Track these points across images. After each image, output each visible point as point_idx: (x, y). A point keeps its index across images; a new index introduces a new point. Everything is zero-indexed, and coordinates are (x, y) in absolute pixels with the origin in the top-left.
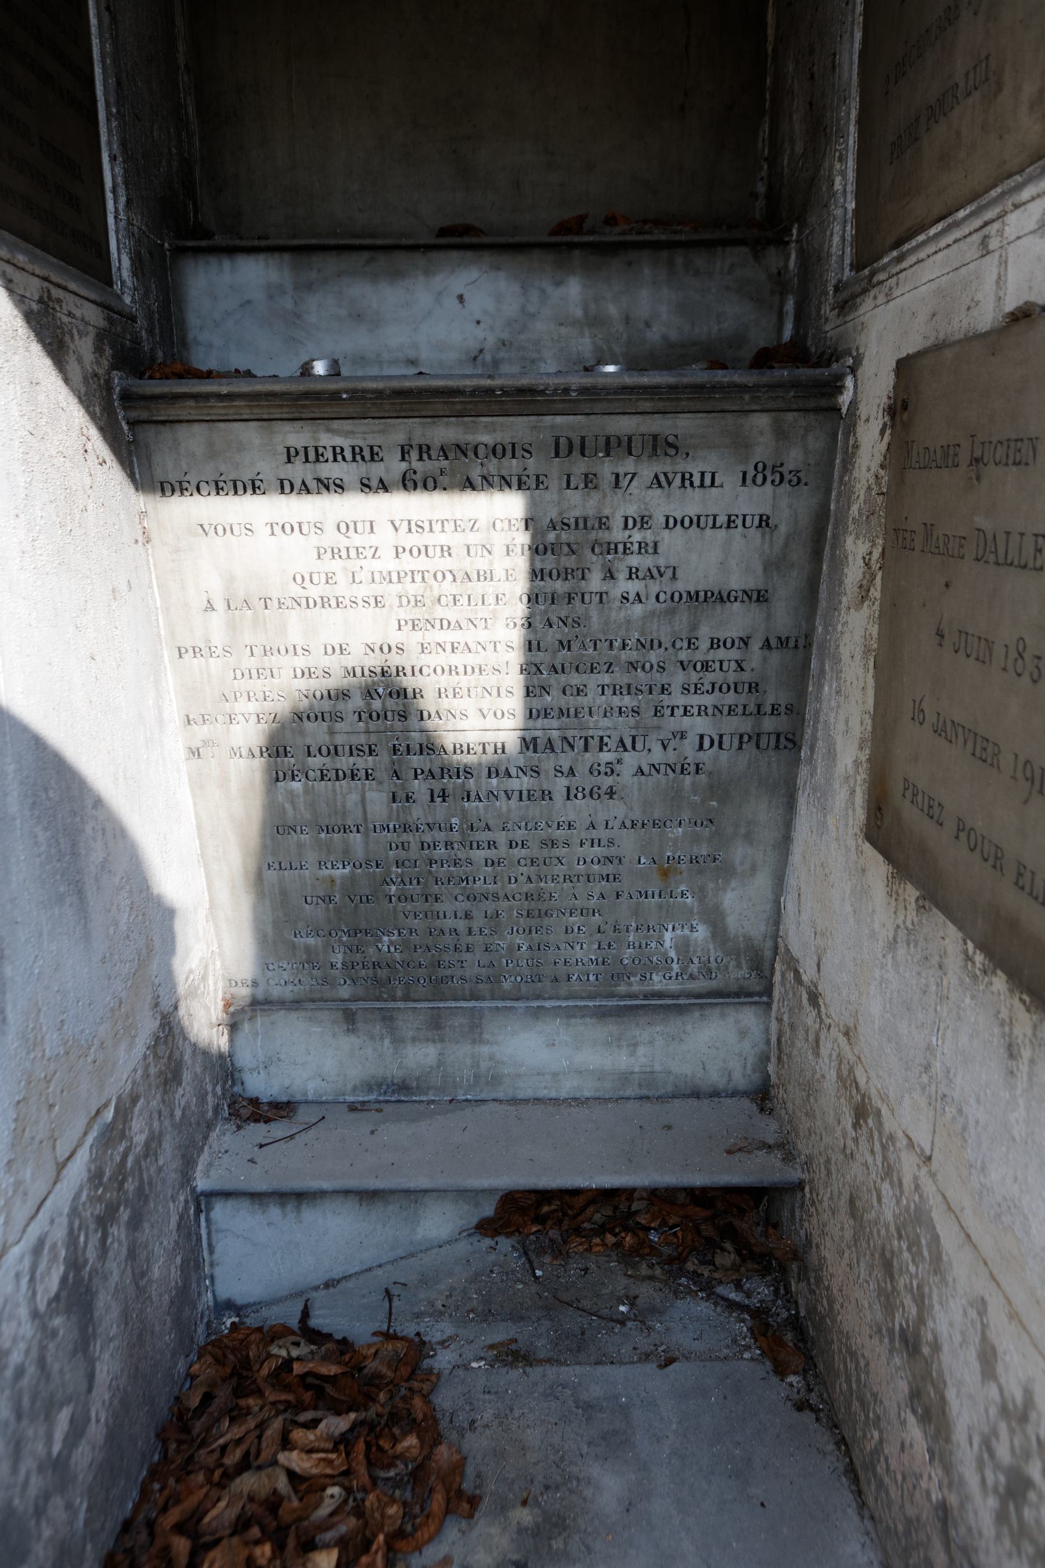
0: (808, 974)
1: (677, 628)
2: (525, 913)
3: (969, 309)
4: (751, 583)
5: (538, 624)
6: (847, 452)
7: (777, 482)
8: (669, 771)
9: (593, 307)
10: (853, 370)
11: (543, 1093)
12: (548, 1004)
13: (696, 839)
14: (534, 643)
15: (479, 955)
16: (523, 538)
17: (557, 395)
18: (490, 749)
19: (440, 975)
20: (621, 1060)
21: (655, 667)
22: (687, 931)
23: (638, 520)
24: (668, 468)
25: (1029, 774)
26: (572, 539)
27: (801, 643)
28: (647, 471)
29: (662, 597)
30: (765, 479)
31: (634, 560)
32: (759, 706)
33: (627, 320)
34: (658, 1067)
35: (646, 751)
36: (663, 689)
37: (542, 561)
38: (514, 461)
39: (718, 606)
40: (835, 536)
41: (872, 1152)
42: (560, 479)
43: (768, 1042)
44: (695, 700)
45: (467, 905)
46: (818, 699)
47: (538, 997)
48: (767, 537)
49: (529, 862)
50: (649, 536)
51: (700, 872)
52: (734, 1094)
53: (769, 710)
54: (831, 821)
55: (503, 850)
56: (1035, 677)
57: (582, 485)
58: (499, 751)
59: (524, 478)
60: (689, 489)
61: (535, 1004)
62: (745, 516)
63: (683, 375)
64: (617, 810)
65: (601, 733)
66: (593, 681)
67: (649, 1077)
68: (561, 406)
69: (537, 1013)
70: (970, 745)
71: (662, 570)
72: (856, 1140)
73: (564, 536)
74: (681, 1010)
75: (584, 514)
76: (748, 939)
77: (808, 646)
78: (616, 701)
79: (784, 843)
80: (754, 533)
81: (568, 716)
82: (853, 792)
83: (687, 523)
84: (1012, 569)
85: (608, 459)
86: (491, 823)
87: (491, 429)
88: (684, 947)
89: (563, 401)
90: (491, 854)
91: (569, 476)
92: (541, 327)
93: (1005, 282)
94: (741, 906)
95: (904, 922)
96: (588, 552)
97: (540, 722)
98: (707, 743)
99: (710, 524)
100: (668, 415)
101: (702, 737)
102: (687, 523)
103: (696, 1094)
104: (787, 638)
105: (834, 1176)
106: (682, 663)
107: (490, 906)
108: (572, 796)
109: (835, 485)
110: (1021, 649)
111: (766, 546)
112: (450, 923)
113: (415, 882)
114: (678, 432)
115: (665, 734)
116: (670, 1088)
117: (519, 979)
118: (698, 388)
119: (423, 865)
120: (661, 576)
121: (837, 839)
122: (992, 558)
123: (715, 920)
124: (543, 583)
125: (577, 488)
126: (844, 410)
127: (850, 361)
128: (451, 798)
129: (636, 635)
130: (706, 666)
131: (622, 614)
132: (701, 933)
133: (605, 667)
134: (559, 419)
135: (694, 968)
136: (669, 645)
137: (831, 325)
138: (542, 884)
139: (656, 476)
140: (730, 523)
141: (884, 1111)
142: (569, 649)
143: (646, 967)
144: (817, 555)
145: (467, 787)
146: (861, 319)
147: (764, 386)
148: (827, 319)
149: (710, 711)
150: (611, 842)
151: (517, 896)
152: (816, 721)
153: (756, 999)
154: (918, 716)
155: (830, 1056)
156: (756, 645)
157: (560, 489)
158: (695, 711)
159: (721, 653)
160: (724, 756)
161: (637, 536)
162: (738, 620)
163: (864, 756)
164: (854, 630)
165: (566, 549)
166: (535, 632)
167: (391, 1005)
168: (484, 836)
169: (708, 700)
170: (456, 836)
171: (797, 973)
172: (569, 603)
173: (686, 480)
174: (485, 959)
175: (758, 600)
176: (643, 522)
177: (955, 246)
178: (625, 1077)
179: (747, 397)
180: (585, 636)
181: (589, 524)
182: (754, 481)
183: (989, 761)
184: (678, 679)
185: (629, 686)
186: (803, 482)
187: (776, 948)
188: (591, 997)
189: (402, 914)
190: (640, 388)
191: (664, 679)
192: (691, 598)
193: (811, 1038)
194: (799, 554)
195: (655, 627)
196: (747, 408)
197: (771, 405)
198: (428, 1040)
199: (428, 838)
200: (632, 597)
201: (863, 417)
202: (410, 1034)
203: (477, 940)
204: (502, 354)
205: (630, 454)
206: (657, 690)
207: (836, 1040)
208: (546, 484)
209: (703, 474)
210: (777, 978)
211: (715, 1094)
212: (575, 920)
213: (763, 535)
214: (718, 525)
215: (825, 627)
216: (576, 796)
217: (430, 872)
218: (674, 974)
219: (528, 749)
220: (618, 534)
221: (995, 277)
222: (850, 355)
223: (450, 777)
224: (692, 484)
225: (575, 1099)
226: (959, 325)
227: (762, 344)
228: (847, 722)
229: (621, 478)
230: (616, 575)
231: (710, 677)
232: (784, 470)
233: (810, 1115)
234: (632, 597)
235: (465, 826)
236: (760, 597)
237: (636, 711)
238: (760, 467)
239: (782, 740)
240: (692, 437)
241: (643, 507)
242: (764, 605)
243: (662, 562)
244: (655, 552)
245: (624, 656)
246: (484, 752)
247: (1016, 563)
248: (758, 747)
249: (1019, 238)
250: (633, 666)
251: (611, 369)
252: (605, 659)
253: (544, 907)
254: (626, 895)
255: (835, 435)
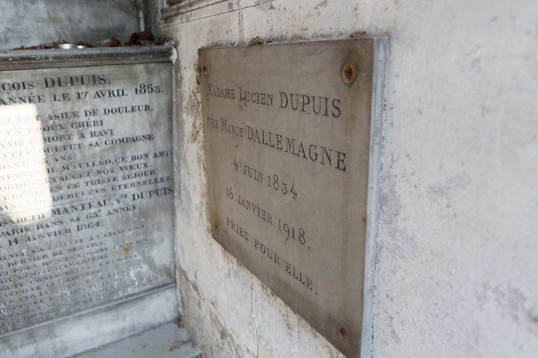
0: (191, 278)
1: (116, 154)
2: (66, 280)
3: (227, 32)
4: (146, 132)
5: (51, 160)
6: (177, 79)
7: (150, 91)
8: (122, 210)
9: (52, 14)
10: (176, 46)
11: (88, 348)
12: (84, 313)
13: (137, 234)
14: (50, 169)
15: (47, 302)
16: (38, 125)
17: (42, 60)
18: (36, 217)
19: (29, 316)
20: (121, 324)
21: (109, 171)
22: (139, 269)
23: (92, 112)
24: (102, 89)
25: (287, 229)
26: (61, 123)
27: (169, 153)
28: (92, 91)
29: (108, 143)
30: (145, 91)
31: (93, 129)
32: (156, 180)
33: (70, 20)
34: (135, 323)
35: (111, 205)
36: (114, 179)
37: (48, 134)
38: (25, 90)
39: (133, 143)
40: (177, 112)
41: (231, 349)
42: (50, 97)
43: (177, 300)
44: (128, 182)
45: (37, 284)
46: (179, 174)
47: (79, 310)
48: (149, 114)
49: (64, 259)
50: (98, 118)
51: (141, 246)
52: (168, 323)
53: (160, 180)
54: (193, 223)
55: (51, 258)
56: (285, 192)
57: (62, 99)
58: (41, 217)
59: (32, 98)
60: (113, 97)
61: (77, 314)
62: (139, 107)
63: (102, 50)
64: (102, 230)
65: (89, 201)
66: (82, 181)
67: (133, 327)
68: (45, 64)
69: (80, 318)
70: (256, 211)
71: (106, 131)
72: (223, 344)
73: (57, 122)
74: (141, 298)
75: (65, 111)
76: (164, 265)
77: (172, 154)
78: (94, 187)
79: (173, 228)
80: (144, 113)
81: (73, 197)
82: (201, 214)
83: (114, 111)
84: (267, 146)
85: (72, 87)
86: (43, 248)
87: (11, 76)
88: (139, 276)
89: (46, 62)
90: (46, 260)
91: (55, 96)
92: (27, 23)
93: (243, 24)
94: (160, 255)
95: (233, 268)
96: (70, 128)
97: (59, 202)
98: (136, 197)
99: (124, 110)
100: (98, 67)
101: (134, 195)
102: (114, 111)
103: (153, 328)
104: (163, 152)
105: (215, 354)
106: (121, 168)
107: (49, 282)
108: (80, 229)
109: (174, 91)
110: (276, 180)
111: (150, 117)
112: (30, 293)
113: (8, 281)
114: (104, 74)
115: (118, 197)
116: (142, 329)
117: (68, 306)
118: (111, 55)
119: (11, 273)
120: (106, 134)
121: (197, 230)
122: (257, 140)
123: (150, 262)
124: (50, 143)
125: (60, 100)
126: (174, 62)
127: (174, 43)
128: (20, 242)
129: (99, 159)
130: (131, 167)
131: (91, 152)
132: (145, 268)
133: (87, 175)
134: (45, 71)
135: (144, 281)
136: (114, 161)
137: (162, 26)
138: (72, 267)
139: (97, 93)
140: (133, 110)
141: (234, 335)
142: (68, 169)
143: (124, 286)
144: (170, 119)
145: (28, 236)
146: (176, 26)
147: (140, 53)
148: (160, 24)
149: (136, 184)
150: (101, 243)
151: (61, 274)
152: (180, 183)
153: (170, 286)
154: (230, 194)
155: (206, 310)
156: (151, 156)
157: (51, 102)
158: (130, 185)
159: (137, 162)
160: (144, 201)
161: (92, 119)
162: (142, 147)
163: (204, 201)
164: (192, 153)
165: (59, 127)
166: (50, 164)
167: (6, 334)
168: (41, 254)
169: (134, 181)
170: (26, 257)
171: (187, 278)
172: (65, 150)
173: (111, 93)
174: (50, 303)
175: (149, 139)
176: (94, 112)
177: (217, 5)
178: (123, 331)
179: (133, 58)
180: (75, 163)
181: (68, 116)
182: (141, 92)
183: (267, 220)
184: (120, 174)
185: (99, 181)
186: (161, 91)
187: (175, 267)
188: (103, 304)
189: (4, 296)
190: (83, 55)
191: (114, 175)
192: (121, 141)
193: (197, 302)
194: (163, 119)
195: (107, 155)
196: (133, 62)
197: (143, 61)
198: (28, 344)
199: (11, 261)
200: (94, 144)
201: (183, 67)
202: (19, 344)
203: (45, 296)
204: (9, 35)
205: (83, 84)
206: (111, 180)
207: (208, 305)
208: (44, 100)
209: (118, 91)
210: (178, 277)
211: (160, 325)
212: (90, 277)
213: (148, 113)
214: (128, 110)
215: (178, 147)
216: (82, 229)
217: (16, 275)
218: (136, 286)
219: (55, 214)
220: (83, 119)
221: (238, 21)
222: (173, 40)
223: (18, 233)
224: (114, 95)
225: (103, 346)
226: (223, 38)
227: (133, 32)
228: (194, 186)
229: (80, 95)
230: (85, 136)
231: (133, 172)
232: (153, 87)
233: (201, 330)
234: (94, 144)
235: (30, 252)
236: (150, 137)
237: (104, 190)
238: (142, 86)
239: (167, 191)
240: (111, 75)
241: (93, 106)
242: (152, 141)
243: (105, 128)
244: (102, 124)
245: (95, 169)
246: (34, 219)
247: (269, 144)
248: (157, 194)
249: (247, 7)
250: (99, 172)
251: (67, 46)
252: (86, 171)
253: (74, 276)
254: (111, 262)
255: (171, 72)
